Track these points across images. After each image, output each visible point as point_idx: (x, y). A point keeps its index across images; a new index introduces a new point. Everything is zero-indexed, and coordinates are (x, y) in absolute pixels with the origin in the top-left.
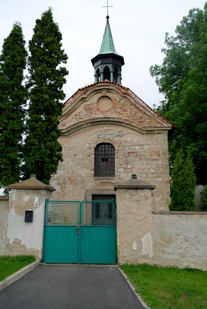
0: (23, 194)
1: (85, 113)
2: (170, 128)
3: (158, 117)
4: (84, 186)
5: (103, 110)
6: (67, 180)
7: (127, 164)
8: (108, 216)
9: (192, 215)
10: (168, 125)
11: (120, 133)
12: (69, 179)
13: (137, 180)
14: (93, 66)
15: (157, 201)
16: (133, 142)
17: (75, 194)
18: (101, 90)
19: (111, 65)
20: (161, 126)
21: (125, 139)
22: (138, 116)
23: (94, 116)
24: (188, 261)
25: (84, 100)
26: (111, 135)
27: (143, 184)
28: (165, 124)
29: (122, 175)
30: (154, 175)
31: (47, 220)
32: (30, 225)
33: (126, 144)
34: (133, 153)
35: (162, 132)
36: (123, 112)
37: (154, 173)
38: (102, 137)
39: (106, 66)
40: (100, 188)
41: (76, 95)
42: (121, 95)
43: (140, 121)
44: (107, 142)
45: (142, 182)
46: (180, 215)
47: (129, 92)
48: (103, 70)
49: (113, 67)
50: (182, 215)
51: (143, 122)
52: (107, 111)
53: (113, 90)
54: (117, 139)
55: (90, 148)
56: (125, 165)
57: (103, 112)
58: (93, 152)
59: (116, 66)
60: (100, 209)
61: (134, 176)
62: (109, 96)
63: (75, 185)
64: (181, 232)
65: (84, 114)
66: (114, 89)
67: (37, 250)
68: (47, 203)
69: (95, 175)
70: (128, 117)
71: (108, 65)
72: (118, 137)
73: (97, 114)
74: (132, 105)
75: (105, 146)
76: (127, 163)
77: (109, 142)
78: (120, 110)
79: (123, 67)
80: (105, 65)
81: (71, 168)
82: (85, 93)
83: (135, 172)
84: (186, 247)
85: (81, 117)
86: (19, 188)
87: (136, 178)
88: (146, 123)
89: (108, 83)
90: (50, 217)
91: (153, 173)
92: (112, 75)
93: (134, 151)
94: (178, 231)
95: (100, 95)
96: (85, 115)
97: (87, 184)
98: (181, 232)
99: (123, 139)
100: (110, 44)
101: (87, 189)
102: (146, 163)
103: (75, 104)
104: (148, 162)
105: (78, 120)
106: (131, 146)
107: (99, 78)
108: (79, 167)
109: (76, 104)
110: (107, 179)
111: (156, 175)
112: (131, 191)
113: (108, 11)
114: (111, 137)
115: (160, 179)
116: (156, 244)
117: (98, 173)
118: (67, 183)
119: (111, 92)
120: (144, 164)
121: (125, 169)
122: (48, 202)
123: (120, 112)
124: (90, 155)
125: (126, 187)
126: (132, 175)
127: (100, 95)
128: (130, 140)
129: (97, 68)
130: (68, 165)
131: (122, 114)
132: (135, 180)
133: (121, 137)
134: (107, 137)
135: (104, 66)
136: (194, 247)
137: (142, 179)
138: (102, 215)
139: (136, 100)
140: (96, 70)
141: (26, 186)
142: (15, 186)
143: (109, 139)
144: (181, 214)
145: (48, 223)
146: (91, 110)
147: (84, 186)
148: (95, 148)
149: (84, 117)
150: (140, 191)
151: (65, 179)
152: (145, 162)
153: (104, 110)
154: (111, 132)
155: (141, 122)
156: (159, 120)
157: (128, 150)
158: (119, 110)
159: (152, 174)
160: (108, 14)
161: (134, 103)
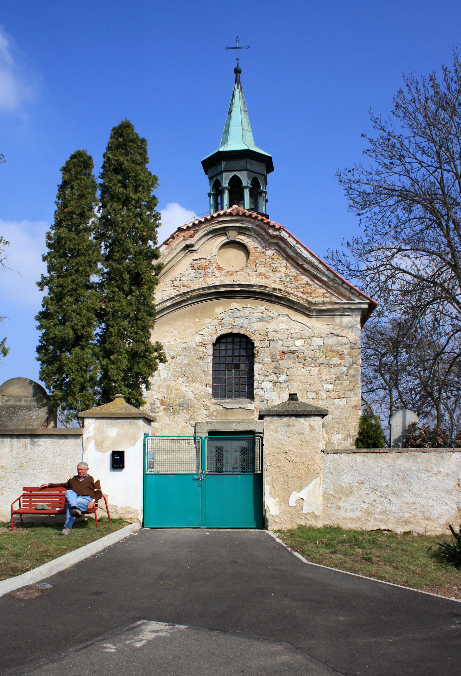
0: (106, 426)
1: (193, 275)
2: (366, 306)
3: (342, 284)
4: (191, 415)
5: (229, 270)
6: (158, 404)
7: (278, 374)
8: (239, 469)
9: (384, 454)
10: (362, 300)
11: (264, 315)
12: (162, 403)
13: (297, 402)
14: (206, 174)
15: (335, 442)
16: (292, 332)
17: (174, 430)
18: (226, 229)
19: (245, 173)
20: (347, 302)
21: (275, 326)
22: (302, 282)
23: (211, 281)
24: (376, 519)
25: (190, 249)
26: (246, 317)
27: (309, 409)
28: (356, 299)
29: (269, 393)
30: (331, 394)
31: (148, 464)
32: (118, 474)
33: (277, 337)
34: (290, 353)
35: (350, 313)
36: (271, 274)
37: (332, 389)
38: (226, 322)
39: (235, 176)
40: (224, 419)
41: (174, 238)
42: (268, 240)
43: (305, 290)
44: (238, 332)
45: (305, 404)
46: (367, 454)
47: (283, 234)
48: (229, 184)
49: (249, 177)
50: (370, 455)
51: (311, 293)
52: (237, 272)
53: (251, 229)
54: (257, 326)
55: (203, 345)
56: (273, 377)
57: (228, 273)
58: (210, 352)
59: (256, 175)
60: (225, 457)
61: (293, 397)
62: (242, 242)
63: (174, 413)
64: (367, 479)
65: (190, 278)
66: (252, 228)
67: (135, 509)
68: (146, 439)
69: (216, 395)
70: (281, 284)
71: (238, 174)
72: (260, 322)
73: (216, 277)
74: (289, 260)
75: (233, 340)
76: (277, 371)
77: (243, 333)
78: (266, 269)
79: (270, 176)
80: (232, 174)
81: (164, 382)
82: (192, 236)
83: (293, 390)
84: (373, 499)
85: (185, 283)
86: (99, 416)
87: (297, 399)
88: (316, 295)
89: (241, 216)
90: (153, 460)
91: (330, 390)
92: (247, 194)
93: (293, 349)
94: (361, 478)
95: (223, 239)
96: (191, 279)
97: (197, 413)
98: (367, 479)
99: (271, 326)
100: (243, 129)
101: (199, 421)
102: (316, 372)
103: (172, 257)
104: (319, 370)
105: (177, 288)
106: (287, 340)
107: (220, 197)
108: (181, 379)
109: (174, 257)
110: (239, 403)
111: (336, 394)
112: (286, 420)
113: (241, 67)
114: (247, 322)
115: (343, 402)
116: (326, 497)
117: (220, 390)
118: (157, 410)
119: (246, 233)
120: (312, 373)
121: (274, 383)
122: (148, 438)
123: (264, 272)
124: (204, 357)
125: (280, 414)
126: (290, 395)
127: (223, 239)
128: (284, 327)
129: (215, 179)
130: (160, 376)
131: (268, 277)
132: (295, 402)
133: (266, 321)
134: (239, 322)
135: (231, 174)
136: (385, 500)
137: (307, 398)
138: (228, 468)
139: (298, 250)
140: (213, 183)
141: (112, 413)
142: (92, 413)
143: (241, 327)
144: (367, 453)
145: (150, 470)
146: (205, 269)
147: (191, 415)
148: (213, 344)
149: (190, 283)
150: (302, 420)
151: (154, 404)
152: (315, 371)
153: (231, 269)
154: (246, 312)
155: (308, 293)
156: (344, 290)
157: (279, 346)
158: (261, 269)
159: (328, 393)
160: (238, 64)
161: (294, 255)
